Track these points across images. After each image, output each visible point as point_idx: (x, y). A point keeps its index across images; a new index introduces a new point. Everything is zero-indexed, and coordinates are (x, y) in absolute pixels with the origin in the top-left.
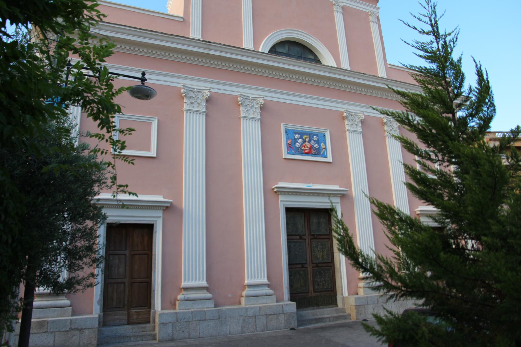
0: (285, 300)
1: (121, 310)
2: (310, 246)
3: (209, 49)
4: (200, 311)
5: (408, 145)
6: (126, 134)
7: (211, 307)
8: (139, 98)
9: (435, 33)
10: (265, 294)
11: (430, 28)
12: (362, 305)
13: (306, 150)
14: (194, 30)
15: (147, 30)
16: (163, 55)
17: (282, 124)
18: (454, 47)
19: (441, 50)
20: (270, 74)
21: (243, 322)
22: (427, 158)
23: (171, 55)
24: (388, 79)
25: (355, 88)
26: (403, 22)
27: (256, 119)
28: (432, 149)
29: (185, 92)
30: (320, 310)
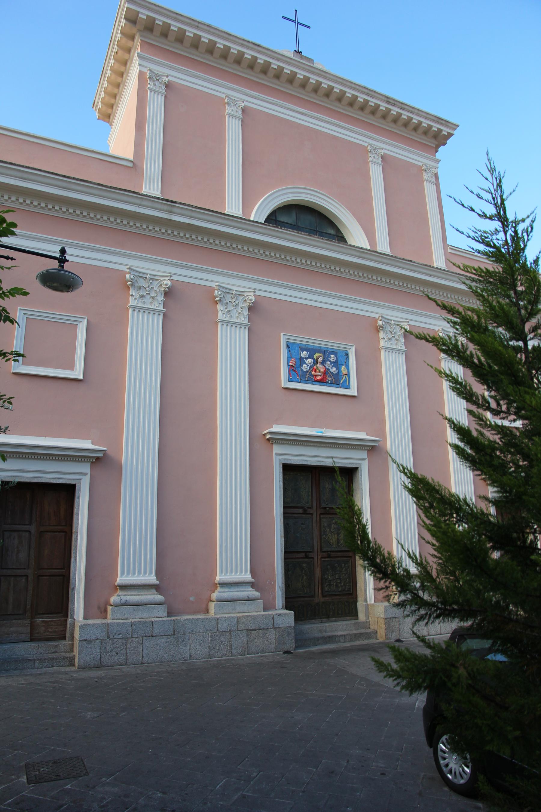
0: (277, 607)
1: (20, 619)
2: (319, 525)
3: (171, 212)
4: (145, 622)
5: (458, 386)
6: (9, 359)
7: (162, 616)
8: (55, 289)
9: (503, 219)
10: (246, 598)
11: (491, 210)
12: (396, 618)
13: (318, 375)
14: (150, 182)
15: (74, 179)
16: (98, 219)
17: (282, 334)
18: (528, 240)
19: (510, 244)
20: (267, 255)
21: (211, 641)
22: (484, 408)
23: (112, 219)
24: (447, 271)
25: (397, 283)
26: (455, 200)
27: (241, 325)
28: (493, 393)
29: (132, 279)
30: (330, 624)
